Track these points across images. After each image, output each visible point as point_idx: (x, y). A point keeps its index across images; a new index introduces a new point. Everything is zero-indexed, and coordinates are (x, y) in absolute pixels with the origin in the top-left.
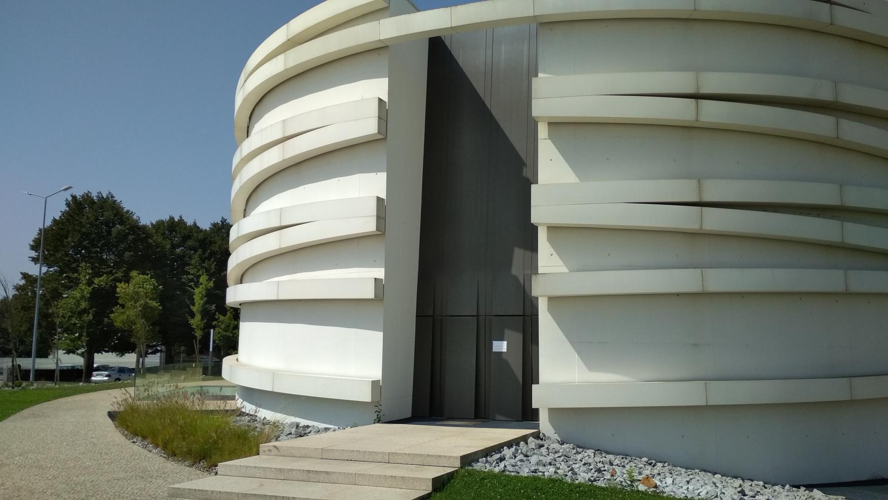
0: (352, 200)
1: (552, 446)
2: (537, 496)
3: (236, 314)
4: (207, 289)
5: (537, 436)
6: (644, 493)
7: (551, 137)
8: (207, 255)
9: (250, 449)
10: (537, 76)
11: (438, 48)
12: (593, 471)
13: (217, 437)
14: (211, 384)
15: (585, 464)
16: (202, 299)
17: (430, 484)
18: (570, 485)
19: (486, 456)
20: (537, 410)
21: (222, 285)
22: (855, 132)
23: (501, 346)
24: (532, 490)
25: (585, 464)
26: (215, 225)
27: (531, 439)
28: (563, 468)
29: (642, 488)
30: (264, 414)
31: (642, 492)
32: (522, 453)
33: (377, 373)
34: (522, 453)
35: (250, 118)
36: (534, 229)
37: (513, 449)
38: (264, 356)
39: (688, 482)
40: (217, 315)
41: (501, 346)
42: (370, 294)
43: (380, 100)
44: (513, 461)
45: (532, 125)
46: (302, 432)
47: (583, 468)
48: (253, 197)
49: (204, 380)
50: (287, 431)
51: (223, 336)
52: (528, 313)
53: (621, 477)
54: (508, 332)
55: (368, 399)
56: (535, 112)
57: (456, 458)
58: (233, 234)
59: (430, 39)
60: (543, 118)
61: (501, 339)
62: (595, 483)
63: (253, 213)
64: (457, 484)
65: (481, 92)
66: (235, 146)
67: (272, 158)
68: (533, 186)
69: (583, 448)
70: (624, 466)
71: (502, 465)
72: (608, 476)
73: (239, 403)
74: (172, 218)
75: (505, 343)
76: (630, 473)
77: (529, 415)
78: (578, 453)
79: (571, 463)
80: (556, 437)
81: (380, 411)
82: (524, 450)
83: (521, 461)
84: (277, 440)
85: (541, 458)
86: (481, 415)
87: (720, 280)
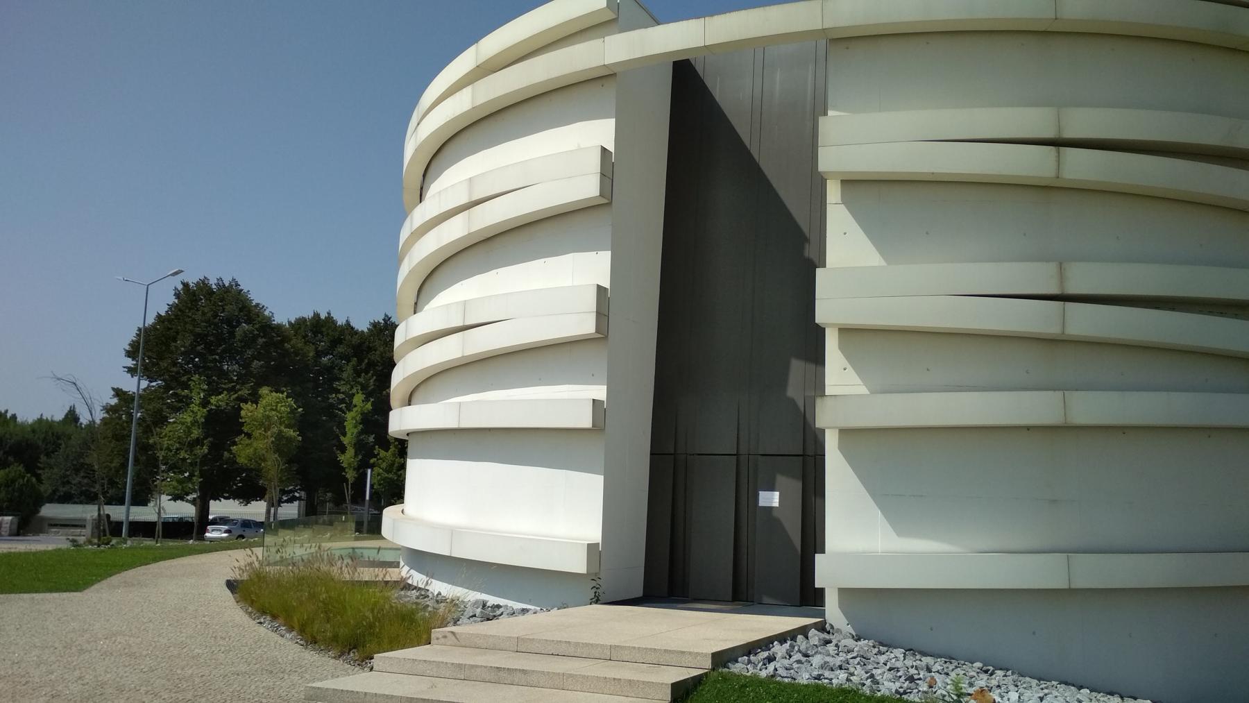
0: (563, 290)
3: (401, 448)
5: (821, 627)
7: (845, 201)
8: (363, 366)
9: (418, 636)
10: (825, 114)
11: (685, 75)
12: (902, 679)
14: (367, 545)
15: (890, 669)
18: (869, 699)
19: (748, 654)
20: (822, 591)
21: (383, 408)
22: (626, 673)
23: (770, 499)
25: (890, 669)
26: (375, 325)
27: (813, 632)
28: (859, 674)
30: (439, 587)
32: (799, 651)
33: (594, 533)
34: (799, 651)
35: (424, 176)
36: (820, 332)
38: (440, 507)
40: (377, 449)
41: (770, 499)
42: (586, 422)
43: (604, 150)
44: (786, 662)
45: (818, 185)
46: (489, 614)
47: (888, 675)
49: (357, 539)
51: (384, 479)
52: (810, 452)
54: (781, 479)
56: (824, 165)
57: (706, 655)
58: (400, 337)
60: (834, 174)
61: (772, 489)
62: (905, 697)
63: (427, 308)
65: (746, 139)
66: (403, 215)
67: (455, 231)
71: (771, 667)
73: (404, 571)
75: (777, 494)
76: (956, 684)
77: (810, 598)
78: (880, 653)
79: (870, 667)
80: (850, 629)
81: (600, 587)
82: (803, 648)
83: (799, 662)
84: (455, 624)
85: (828, 659)
86: (741, 595)
87: (1091, 408)
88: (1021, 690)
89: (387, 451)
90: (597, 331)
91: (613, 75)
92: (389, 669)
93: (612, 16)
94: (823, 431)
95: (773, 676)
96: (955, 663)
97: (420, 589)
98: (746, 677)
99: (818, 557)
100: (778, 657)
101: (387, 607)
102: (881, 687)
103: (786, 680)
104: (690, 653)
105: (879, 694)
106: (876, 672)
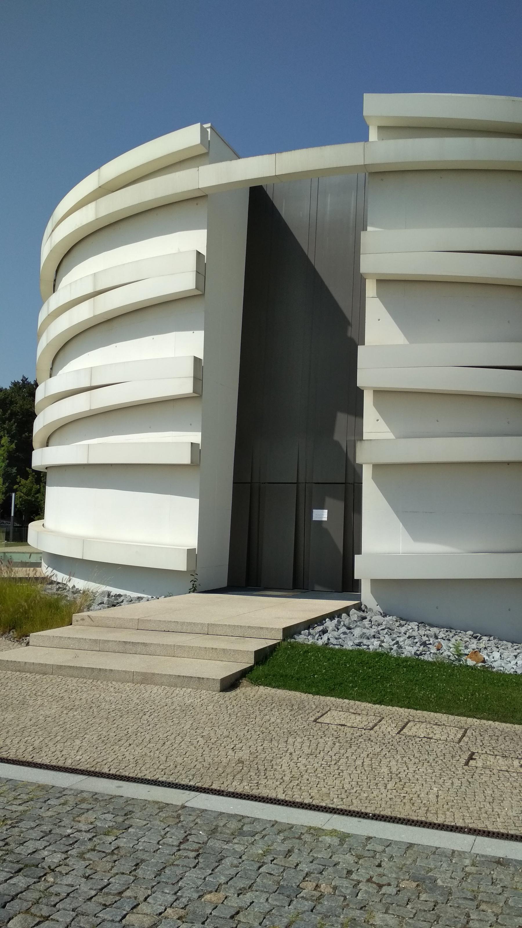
0: (167, 360)
1: (374, 618)
2: (363, 670)
3: (40, 478)
4: (9, 452)
5: (358, 607)
6: (473, 668)
7: (379, 295)
8: (7, 415)
9: (63, 619)
10: (365, 229)
11: (259, 199)
12: (418, 644)
13: (29, 607)
14: (15, 551)
15: (409, 637)
16: (3, 461)
17: (252, 656)
18: (397, 659)
19: (308, 628)
20: (358, 582)
21: (25, 448)
23: (322, 515)
24: (358, 664)
25: (409, 637)
26: (15, 384)
27: (353, 611)
28: (388, 642)
29: (470, 662)
30: (80, 584)
31: (470, 667)
32: (344, 625)
33: (193, 542)
34: (344, 625)
35: (57, 271)
36: (360, 393)
37: (335, 621)
38: (73, 523)
39: (516, 657)
40: (19, 479)
41: (322, 515)
42: (186, 459)
43: (198, 254)
44: (336, 634)
45: (359, 282)
46: (114, 602)
47: (408, 642)
48: (61, 355)
49: (6, 546)
50: (99, 600)
51: (25, 500)
52: (350, 481)
53: (448, 651)
54: (329, 501)
55: (183, 567)
56: (364, 269)
57: (278, 629)
58: (40, 394)
59: (250, 188)
60: (371, 275)
61: (322, 508)
62: (422, 657)
63: (60, 372)
64: (280, 657)
66: (41, 302)
67: (83, 313)
68: (360, 348)
69: (407, 620)
70: (449, 640)
71: (325, 637)
72: (433, 650)
73: (45, 570)
74: (24, 380)
75: (326, 512)
76: (457, 647)
77: (348, 585)
78: (401, 625)
79: (395, 636)
80: (378, 609)
81: (197, 580)
82: (347, 622)
83: (345, 633)
84: (89, 610)
85: (365, 631)
86: (299, 585)
88: (501, 651)
89: (26, 479)
90: (195, 391)
91: (205, 196)
92: (41, 644)
93: (204, 150)
94: (361, 466)
95: (327, 644)
96: (454, 632)
97: (58, 583)
98: (308, 645)
99: (357, 557)
100: (330, 629)
101: (38, 598)
102: (404, 650)
103: (337, 647)
104: (267, 628)
105: (403, 656)
106: (400, 639)
